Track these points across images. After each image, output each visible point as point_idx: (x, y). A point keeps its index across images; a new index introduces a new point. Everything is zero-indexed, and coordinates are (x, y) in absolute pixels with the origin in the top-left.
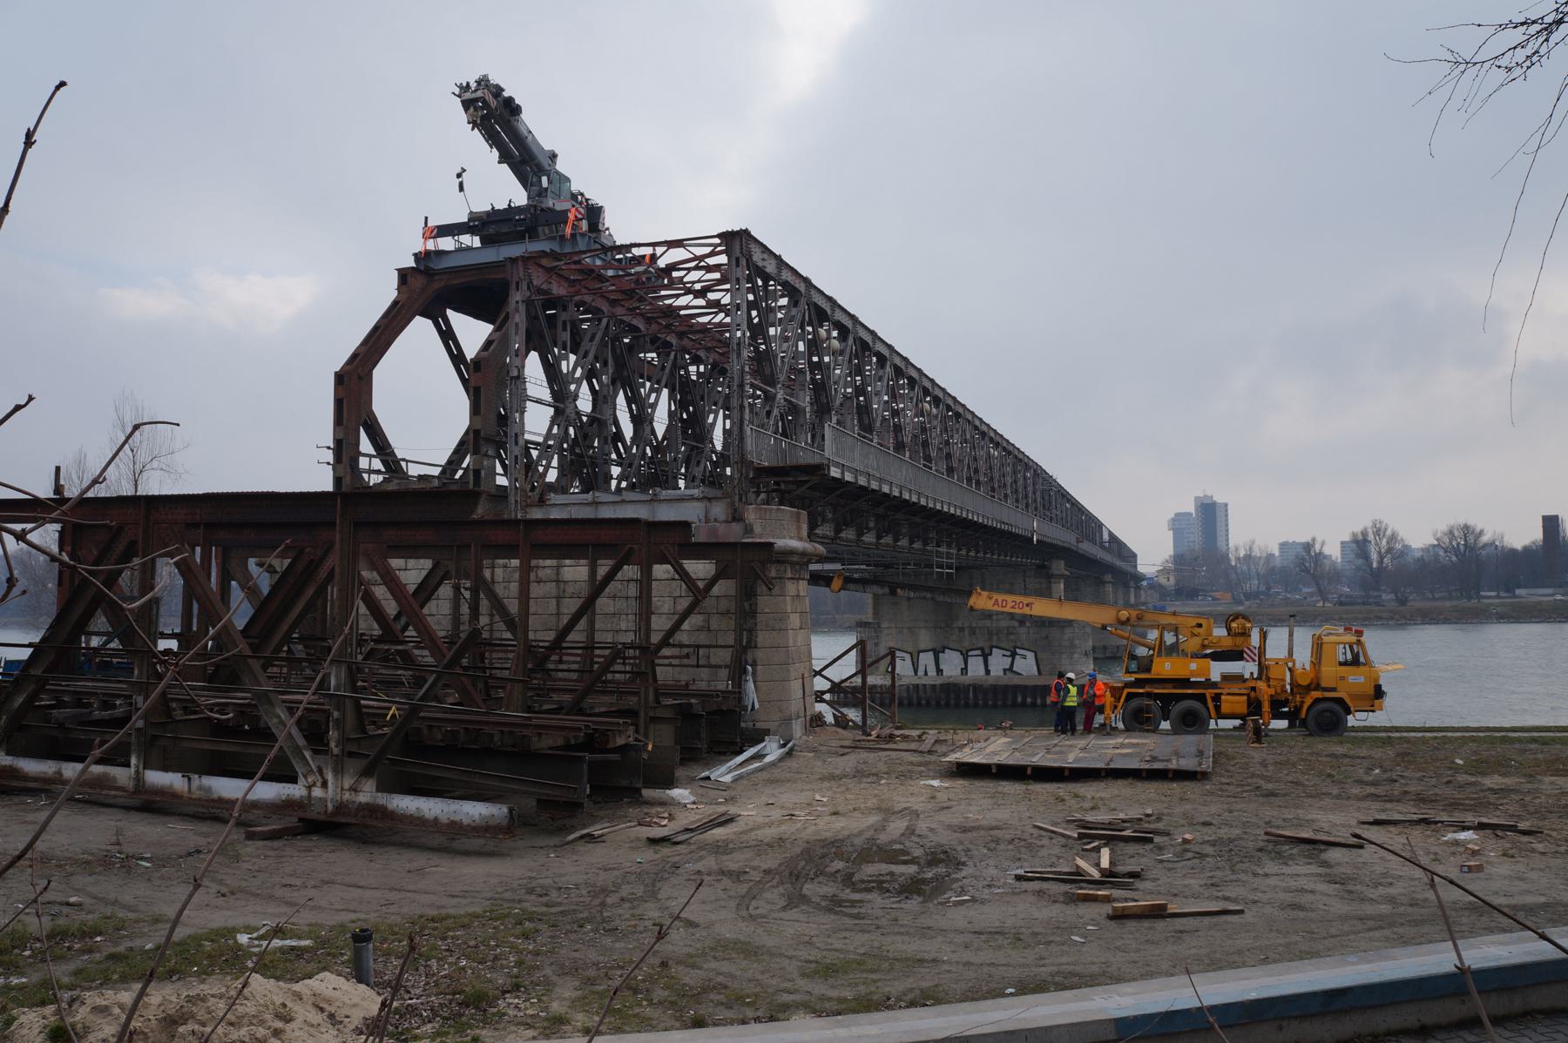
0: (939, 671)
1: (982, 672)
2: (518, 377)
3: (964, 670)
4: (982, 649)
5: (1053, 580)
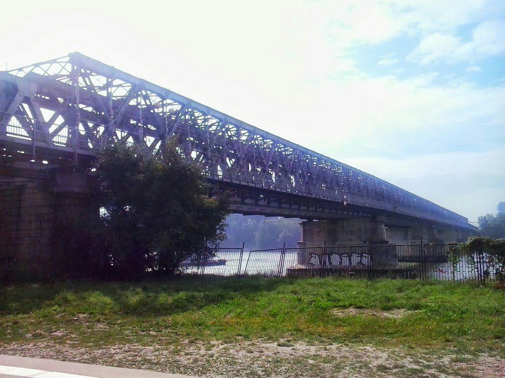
0: (330, 263)
1: (348, 264)
2: (332, 164)
3: (341, 263)
4: (348, 254)
5: (378, 224)
